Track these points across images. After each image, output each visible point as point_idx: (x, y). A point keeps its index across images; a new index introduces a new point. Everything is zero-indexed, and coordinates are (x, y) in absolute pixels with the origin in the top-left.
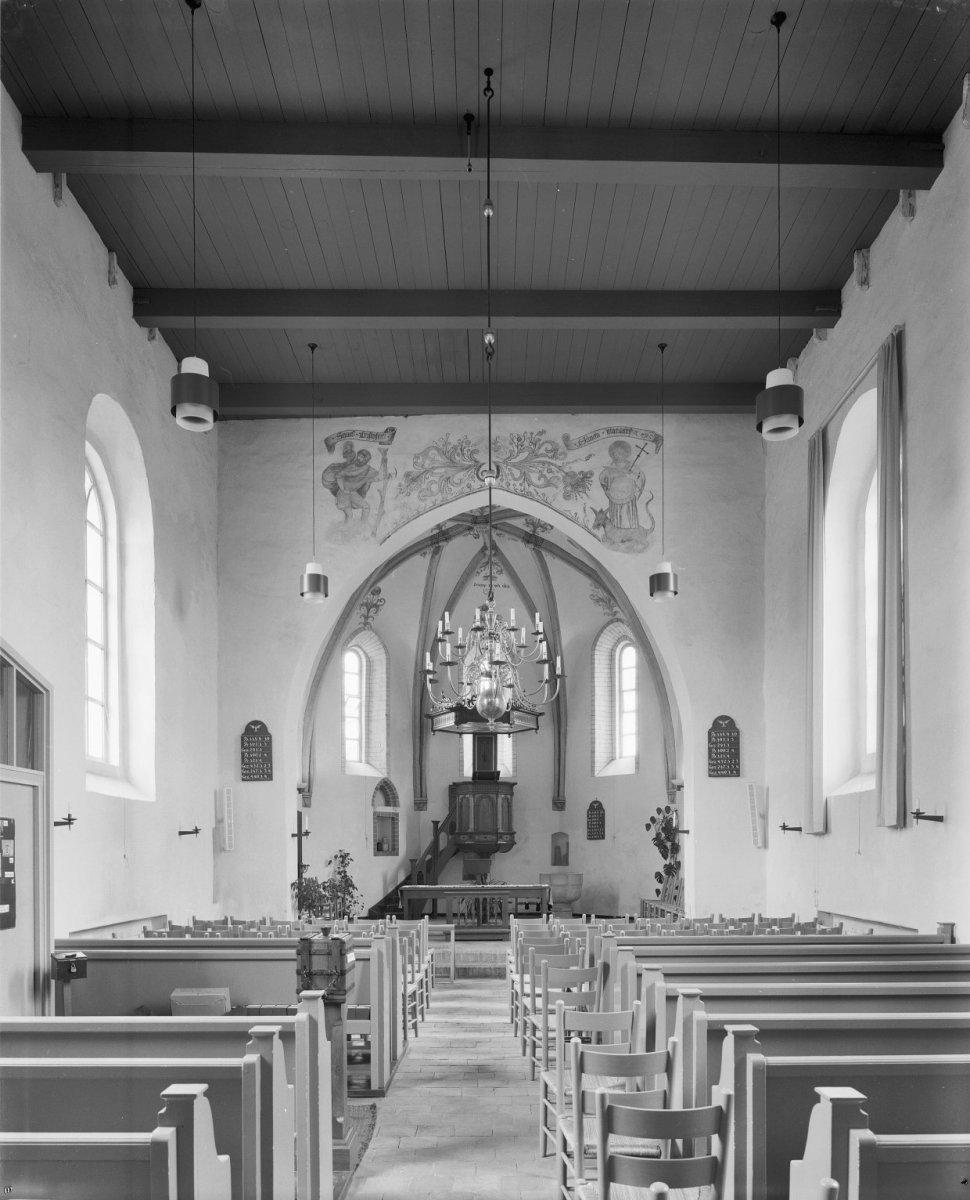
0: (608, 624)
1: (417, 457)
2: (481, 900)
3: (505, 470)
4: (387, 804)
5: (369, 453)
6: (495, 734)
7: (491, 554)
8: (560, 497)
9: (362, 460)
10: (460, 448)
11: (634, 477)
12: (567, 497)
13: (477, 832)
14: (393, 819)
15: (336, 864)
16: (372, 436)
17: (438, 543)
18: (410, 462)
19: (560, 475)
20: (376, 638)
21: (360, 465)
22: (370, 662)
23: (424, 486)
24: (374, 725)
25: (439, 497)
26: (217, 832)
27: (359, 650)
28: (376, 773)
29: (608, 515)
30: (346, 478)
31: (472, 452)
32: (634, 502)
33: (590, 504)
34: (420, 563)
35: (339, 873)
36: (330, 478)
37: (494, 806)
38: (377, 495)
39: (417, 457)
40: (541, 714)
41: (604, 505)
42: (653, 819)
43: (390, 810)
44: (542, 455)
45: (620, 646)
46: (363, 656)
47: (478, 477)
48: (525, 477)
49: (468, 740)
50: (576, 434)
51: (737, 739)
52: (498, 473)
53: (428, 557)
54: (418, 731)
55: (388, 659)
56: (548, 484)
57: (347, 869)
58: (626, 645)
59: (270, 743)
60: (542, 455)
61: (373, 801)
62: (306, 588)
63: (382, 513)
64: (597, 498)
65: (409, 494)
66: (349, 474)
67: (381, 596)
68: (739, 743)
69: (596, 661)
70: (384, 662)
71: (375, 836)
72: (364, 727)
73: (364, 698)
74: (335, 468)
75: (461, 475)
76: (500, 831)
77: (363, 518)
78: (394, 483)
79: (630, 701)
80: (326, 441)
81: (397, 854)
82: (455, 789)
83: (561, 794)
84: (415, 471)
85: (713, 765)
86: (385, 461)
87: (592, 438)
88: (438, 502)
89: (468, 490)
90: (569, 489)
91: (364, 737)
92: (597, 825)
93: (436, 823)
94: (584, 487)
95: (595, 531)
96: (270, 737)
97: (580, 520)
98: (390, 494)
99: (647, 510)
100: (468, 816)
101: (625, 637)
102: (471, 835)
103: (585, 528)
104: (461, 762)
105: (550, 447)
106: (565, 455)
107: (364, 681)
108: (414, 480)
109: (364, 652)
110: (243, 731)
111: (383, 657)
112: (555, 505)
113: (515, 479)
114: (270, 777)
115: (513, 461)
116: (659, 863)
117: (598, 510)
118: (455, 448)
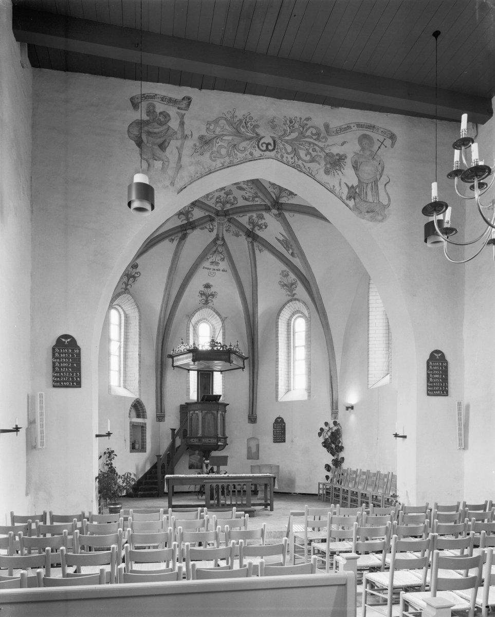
0: (288, 302)
1: (209, 123)
2: (220, 487)
3: (280, 145)
4: (138, 416)
5: (169, 116)
6: (212, 372)
7: (218, 246)
8: (322, 171)
9: (162, 120)
10: (245, 121)
11: (376, 163)
12: (327, 172)
13: (203, 437)
14: (142, 427)
15: (104, 459)
16: (172, 101)
17: (186, 230)
18: (204, 127)
19: (322, 154)
20: (133, 300)
21: (161, 124)
22: (126, 317)
23: (215, 149)
24: (129, 362)
25: (227, 160)
26: (28, 430)
27: (119, 308)
28: (132, 394)
29: (357, 190)
30: (149, 133)
31: (254, 127)
32: (376, 182)
33: (344, 180)
34: (166, 248)
35: (107, 465)
36: (135, 131)
37: (216, 419)
38: (175, 151)
39: (209, 123)
40: (246, 358)
41: (355, 182)
42: (322, 430)
43: (140, 420)
44: (308, 137)
45: (294, 317)
46: (122, 313)
47: (259, 147)
48: (295, 152)
49: (193, 375)
50: (335, 124)
51: (446, 367)
52: (275, 146)
53: (176, 243)
54: (159, 366)
55: (140, 316)
56: (313, 160)
57: (113, 462)
58: (300, 316)
59: (79, 355)
60: (308, 137)
61: (130, 414)
62: (134, 197)
63: (179, 167)
64: (349, 176)
65: (202, 154)
66: (151, 130)
67: (138, 270)
68: (447, 371)
69: (279, 326)
70: (138, 318)
71: (131, 439)
72: (122, 362)
73: (122, 343)
74: (140, 124)
75: (244, 144)
76: (220, 436)
77: (163, 169)
78: (189, 143)
79: (300, 353)
80: (132, 99)
81: (145, 452)
82: (185, 408)
83: (254, 413)
84: (209, 135)
85: (431, 387)
86: (182, 124)
87: (345, 129)
88: (226, 164)
89: (250, 157)
90: (328, 166)
91: (122, 369)
92: (280, 431)
93: (173, 430)
94: (340, 166)
95: (348, 202)
96: (80, 350)
97: (337, 192)
98: (186, 151)
99: (386, 190)
100: (198, 425)
101: (298, 311)
102: (200, 439)
103: (341, 198)
104: (188, 389)
105: (314, 132)
106: (326, 139)
107: (123, 330)
108: (207, 143)
109: (123, 310)
110: (54, 343)
111: (137, 314)
112: (317, 177)
113: (288, 153)
114: (78, 385)
115: (287, 138)
116: (328, 459)
117: (350, 185)
118: (241, 121)
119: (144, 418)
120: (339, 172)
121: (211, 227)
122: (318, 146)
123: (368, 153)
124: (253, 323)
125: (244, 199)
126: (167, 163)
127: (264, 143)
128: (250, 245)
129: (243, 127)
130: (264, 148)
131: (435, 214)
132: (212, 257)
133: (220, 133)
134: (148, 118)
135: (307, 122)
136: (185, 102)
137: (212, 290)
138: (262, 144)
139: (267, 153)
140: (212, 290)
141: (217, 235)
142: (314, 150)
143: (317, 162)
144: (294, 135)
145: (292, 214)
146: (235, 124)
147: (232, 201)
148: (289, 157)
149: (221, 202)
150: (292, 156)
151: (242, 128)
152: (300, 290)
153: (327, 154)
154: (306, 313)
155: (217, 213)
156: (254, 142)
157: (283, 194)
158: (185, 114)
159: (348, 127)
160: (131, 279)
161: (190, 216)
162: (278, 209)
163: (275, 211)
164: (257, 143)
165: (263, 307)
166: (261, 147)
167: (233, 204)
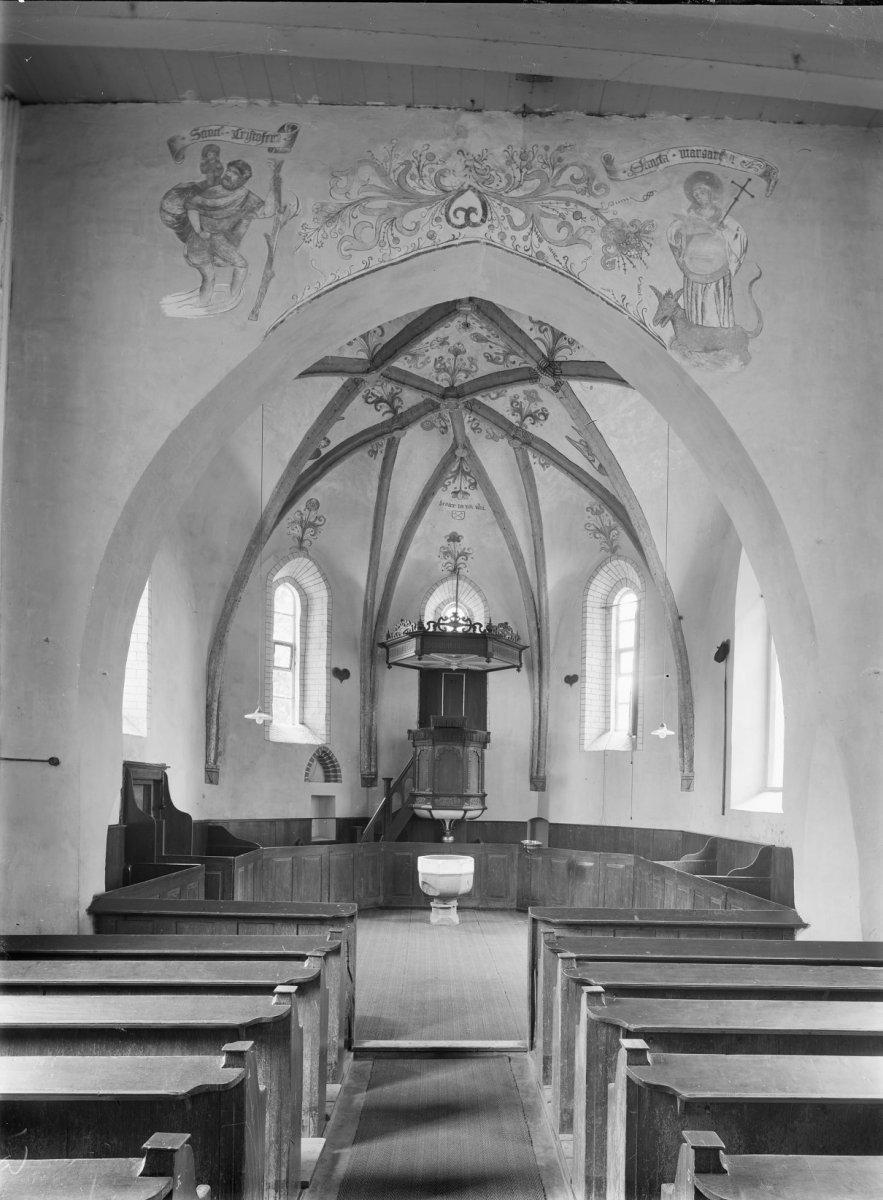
5: (248, 167)
29: (681, 301)
47: (448, 221)
48: (533, 221)
56: (574, 240)
66: (209, 202)
67: (320, 512)
74: (188, 192)
90: (612, 250)
112: (585, 278)
113: (515, 228)
115: (514, 194)
119: (268, 713)
120: (636, 262)
121: (443, 424)
122: (588, 207)
123: (708, 212)
124: (539, 595)
125: (488, 360)
126: (242, 271)
127: (462, 209)
128: (519, 453)
129: (413, 177)
130: (461, 220)
131: (190, 102)
132: (454, 482)
133: (361, 196)
134: (203, 178)
135: (561, 155)
136: (284, 135)
137: (464, 544)
138: (455, 213)
139: (468, 233)
140: (464, 544)
141: (455, 439)
142: (577, 215)
143: (586, 243)
144: (533, 184)
145: (587, 384)
146: (394, 171)
147: (467, 367)
148: (520, 235)
149: (446, 370)
150: (525, 232)
151: (409, 181)
152: (624, 540)
153: (608, 222)
154: (638, 581)
155: (445, 394)
156: (438, 210)
157: (562, 342)
158: (282, 162)
159: (660, 157)
160: (309, 530)
161: (397, 403)
162: (554, 375)
163: (547, 380)
164: (443, 211)
165: (556, 573)
166: (453, 220)
167: (467, 372)
